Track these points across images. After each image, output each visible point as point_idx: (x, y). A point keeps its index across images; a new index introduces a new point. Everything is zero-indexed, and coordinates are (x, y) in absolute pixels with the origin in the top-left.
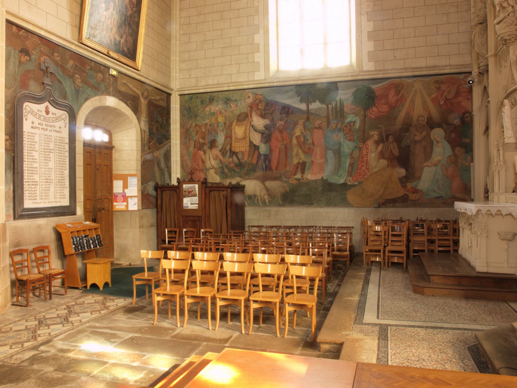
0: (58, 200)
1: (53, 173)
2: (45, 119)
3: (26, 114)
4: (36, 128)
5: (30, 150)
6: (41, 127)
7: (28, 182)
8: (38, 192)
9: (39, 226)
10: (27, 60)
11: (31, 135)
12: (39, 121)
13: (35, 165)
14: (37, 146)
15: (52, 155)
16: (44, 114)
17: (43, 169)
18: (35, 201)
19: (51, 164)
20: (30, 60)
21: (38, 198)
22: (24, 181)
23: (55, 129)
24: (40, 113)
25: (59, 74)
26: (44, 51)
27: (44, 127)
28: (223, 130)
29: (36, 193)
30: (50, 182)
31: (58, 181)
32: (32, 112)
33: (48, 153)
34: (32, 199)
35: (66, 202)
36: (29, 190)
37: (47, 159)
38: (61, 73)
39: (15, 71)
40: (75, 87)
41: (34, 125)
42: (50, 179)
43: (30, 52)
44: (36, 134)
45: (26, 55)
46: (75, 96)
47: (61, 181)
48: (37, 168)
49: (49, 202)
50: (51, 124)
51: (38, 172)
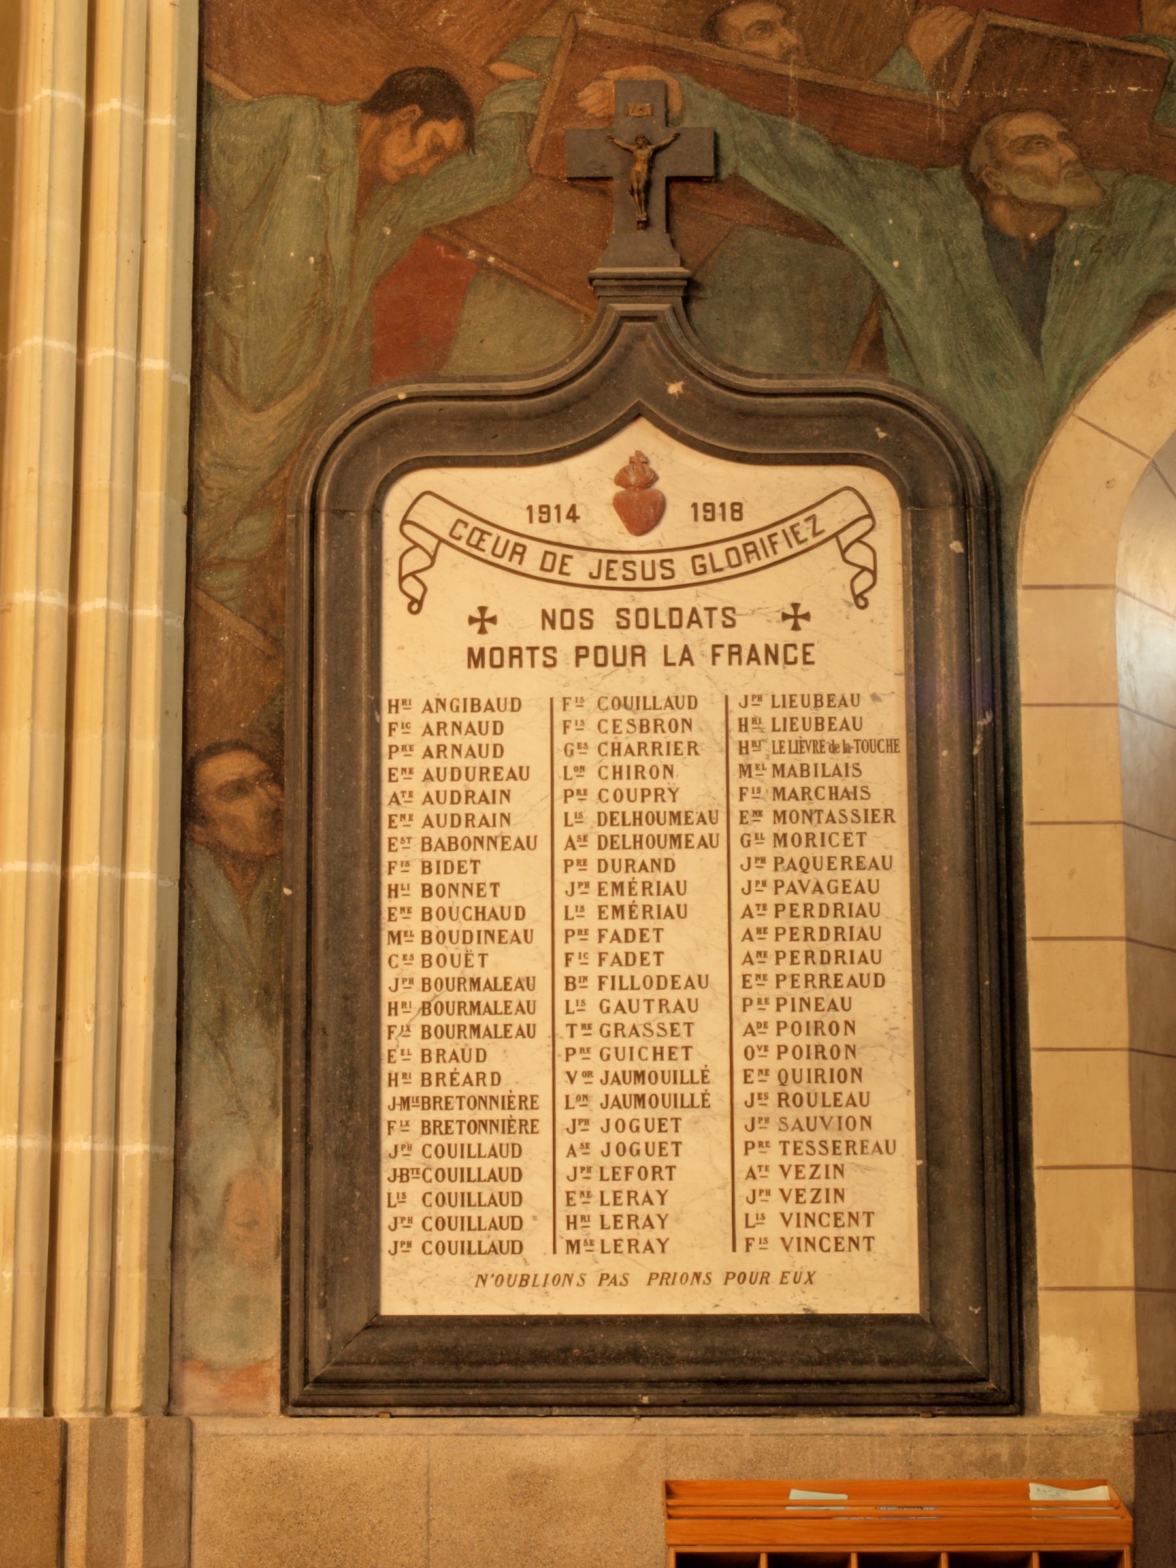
0: (775, 1260)
1: (709, 1026)
2: (612, 569)
3: (416, 560)
4: (515, 654)
5: (453, 844)
6: (565, 641)
7: (428, 1103)
8: (535, 1187)
9: (529, 1486)
10: (436, 149)
11: (465, 718)
12: (554, 598)
13: (505, 961)
14: (527, 808)
15: (697, 867)
16: (606, 527)
17: (591, 994)
18: (507, 1264)
19: (691, 945)
20: (469, 141)
21: (537, 1236)
22: (388, 1094)
23: (727, 637)
24: (563, 531)
25: (800, 171)
26: (611, 29)
27: (605, 633)
28: (980, 168)
29: (517, 1198)
30: (677, 1101)
31: (771, 1086)
32: (476, 538)
33: (647, 855)
34: (466, 1249)
35: (878, 1275)
36: (443, 1174)
37: (639, 902)
38: (816, 154)
39: (324, 261)
40: (992, 232)
41: (497, 636)
42: (677, 1077)
43: (470, 80)
44: (515, 705)
45: (429, 114)
46: (998, 312)
47: (816, 1087)
48: (526, 983)
49: (665, 1278)
50: (686, 600)
51: (541, 1019)
